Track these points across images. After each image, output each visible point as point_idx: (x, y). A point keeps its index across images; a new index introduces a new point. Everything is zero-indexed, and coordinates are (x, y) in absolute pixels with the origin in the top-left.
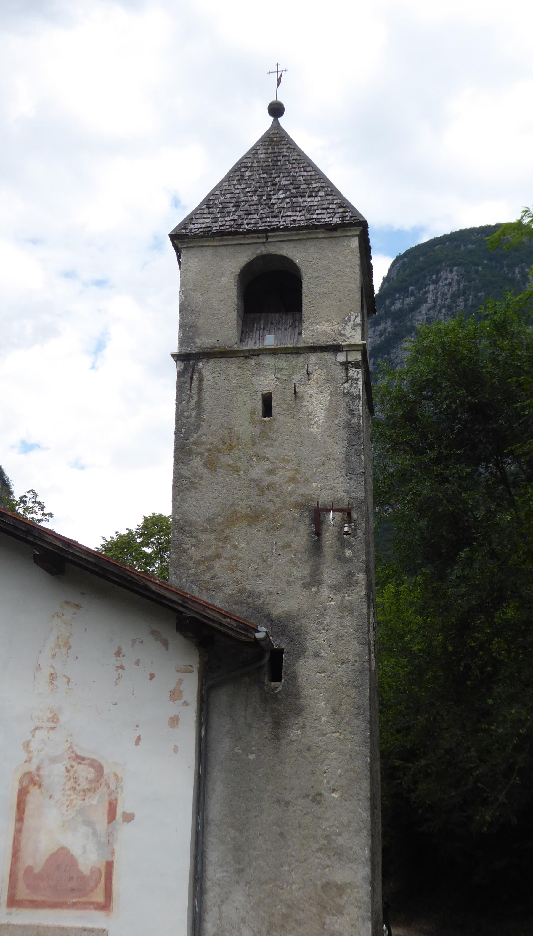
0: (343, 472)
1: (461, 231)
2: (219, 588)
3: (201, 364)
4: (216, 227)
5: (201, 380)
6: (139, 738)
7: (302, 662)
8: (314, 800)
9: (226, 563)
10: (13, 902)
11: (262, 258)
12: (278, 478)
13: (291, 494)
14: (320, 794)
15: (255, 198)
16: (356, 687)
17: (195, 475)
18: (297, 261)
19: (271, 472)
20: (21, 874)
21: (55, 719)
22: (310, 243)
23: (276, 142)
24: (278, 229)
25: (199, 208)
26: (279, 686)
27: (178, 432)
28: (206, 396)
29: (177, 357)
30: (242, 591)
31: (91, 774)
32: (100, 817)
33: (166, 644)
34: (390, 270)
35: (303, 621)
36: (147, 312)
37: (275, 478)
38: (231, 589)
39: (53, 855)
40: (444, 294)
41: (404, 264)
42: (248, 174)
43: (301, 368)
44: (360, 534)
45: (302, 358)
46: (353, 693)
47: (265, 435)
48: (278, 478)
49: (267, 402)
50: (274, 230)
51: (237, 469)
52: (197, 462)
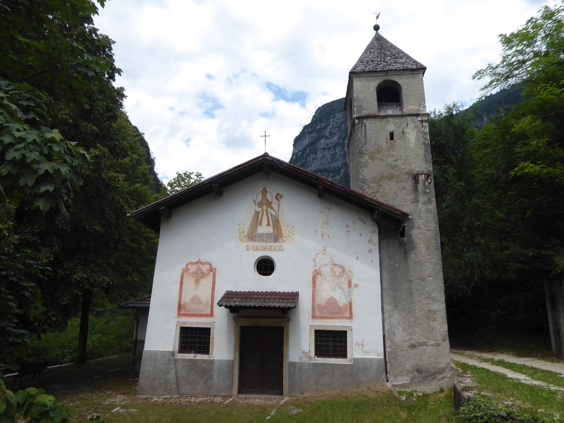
3: (365, 121)
4: (367, 69)
5: (365, 127)
6: (358, 257)
7: (413, 230)
10: (314, 317)
11: (385, 82)
19: (395, 161)
20: (316, 307)
21: (324, 250)
22: (404, 76)
28: (368, 133)
31: (340, 270)
32: (346, 286)
33: (365, 223)
34: (316, 113)
37: (397, 163)
39: (328, 300)
40: (337, 123)
41: (321, 110)
44: (432, 184)
45: (404, 119)
46: (434, 241)
47: (392, 147)
51: (382, 160)
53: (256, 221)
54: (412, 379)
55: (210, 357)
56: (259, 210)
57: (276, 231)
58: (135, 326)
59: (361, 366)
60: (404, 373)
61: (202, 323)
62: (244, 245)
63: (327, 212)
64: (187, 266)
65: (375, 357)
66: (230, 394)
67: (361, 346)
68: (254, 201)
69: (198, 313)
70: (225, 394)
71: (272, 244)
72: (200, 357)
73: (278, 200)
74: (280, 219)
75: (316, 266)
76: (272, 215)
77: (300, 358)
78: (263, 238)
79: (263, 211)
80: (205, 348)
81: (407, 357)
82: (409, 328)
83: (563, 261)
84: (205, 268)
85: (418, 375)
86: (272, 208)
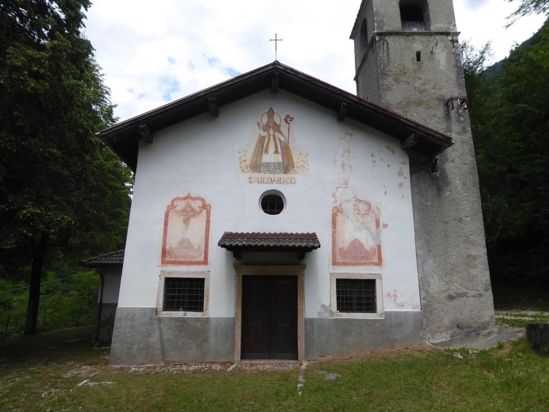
0: (456, 85)
3: (387, 38)
5: (388, 45)
6: (386, 192)
7: (447, 164)
10: (335, 263)
13: (435, 93)
14: (461, 219)
16: (472, 174)
19: (424, 84)
20: (337, 251)
21: (346, 183)
31: (366, 207)
32: (373, 226)
33: (393, 152)
45: (432, 37)
49: (418, 55)
53: (261, 147)
54: (452, 336)
55: (204, 315)
56: (264, 134)
57: (285, 160)
58: (259, 155)
59: (395, 320)
60: (443, 329)
61: (193, 273)
62: (247, 175)
63: (348, 138)
64: (173, 202)
65: (411, 310)
66: (230, 360)
67: (393, 298)
69: (188, 259)
70: (224, 360)
71: (282, 175)
72: (191, 314)
73: (287, 123)
74: (291, 146)
75: (335, 202)
76: (280, 141)
77: (319, 313)
78: (269, 168)
79: (269, 136)
80: (197, 304)
81: (445, 310)
82: (445, 277)
84: (196, 205)
86: (280, 132)
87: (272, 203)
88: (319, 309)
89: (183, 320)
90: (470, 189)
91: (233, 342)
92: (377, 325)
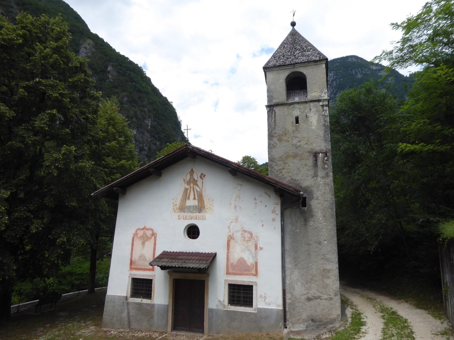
1: (334, 59)
2: (285, 178)
4: (278, 64)
5: (275, 113)
6: (263, 225)
7: (312, 201)
8: (318, 244)
9: (286, 171)
10: (228, 273)
11: (293, 73)
12: (302, 143)
13: (307, 148)
15: (289, 53)
17: (275, 143)
18: (305, 73)
19: (299, 141)
20: (230, 265)
21: (237, 219)
22: (308, 67)
23: (294, 35)
24: (298, 63)
25: (271, 58)
26: (306, 209)
27: (269, 130)
28: (277, 118)
29: (267, 106)
30: (292, 179)
31: (249, 236)
32: (253, 249)
33: (270, 196)
35: (312, 188)
36: (258, 92)
38: (289, 179)
42: (286, 46)
43: (308, 107)
44: (330, 160)
45: (308, 104)
46: (330, 210)
47: (297, 130)
48: (302, 143)
50: (297, 63)
51: (288, 141)
52: (275, 139)
53: (186, 196)
54: (307, 327)
55: (152, 302)
57: (200, 204)
59: (264, 314)
60: (301, 321)
61: (143, 275)
62: (177, 214)
65: (275, 307)
67: (264, 299)
68: (184, 180)
69: (144, 267)
70: (162, 331)
71: (197, 214)
72: (145, 301)
73: (201, 178)
74: (203, 194)
75: (230, 232)
76: (197, 191)
77: (217, 305)
79: (191, 188)
80: (148, 294)
81: (304, 308)
82: (306, 284)
83: (453, 229)
84: (149, 233)
85: (312, 324)
86: (197, 185)
87: (193, 232)
88: (217, 303)
89: (140, 304)
90: (329, 220)
91: (167, 320)
92: (252, 317)
